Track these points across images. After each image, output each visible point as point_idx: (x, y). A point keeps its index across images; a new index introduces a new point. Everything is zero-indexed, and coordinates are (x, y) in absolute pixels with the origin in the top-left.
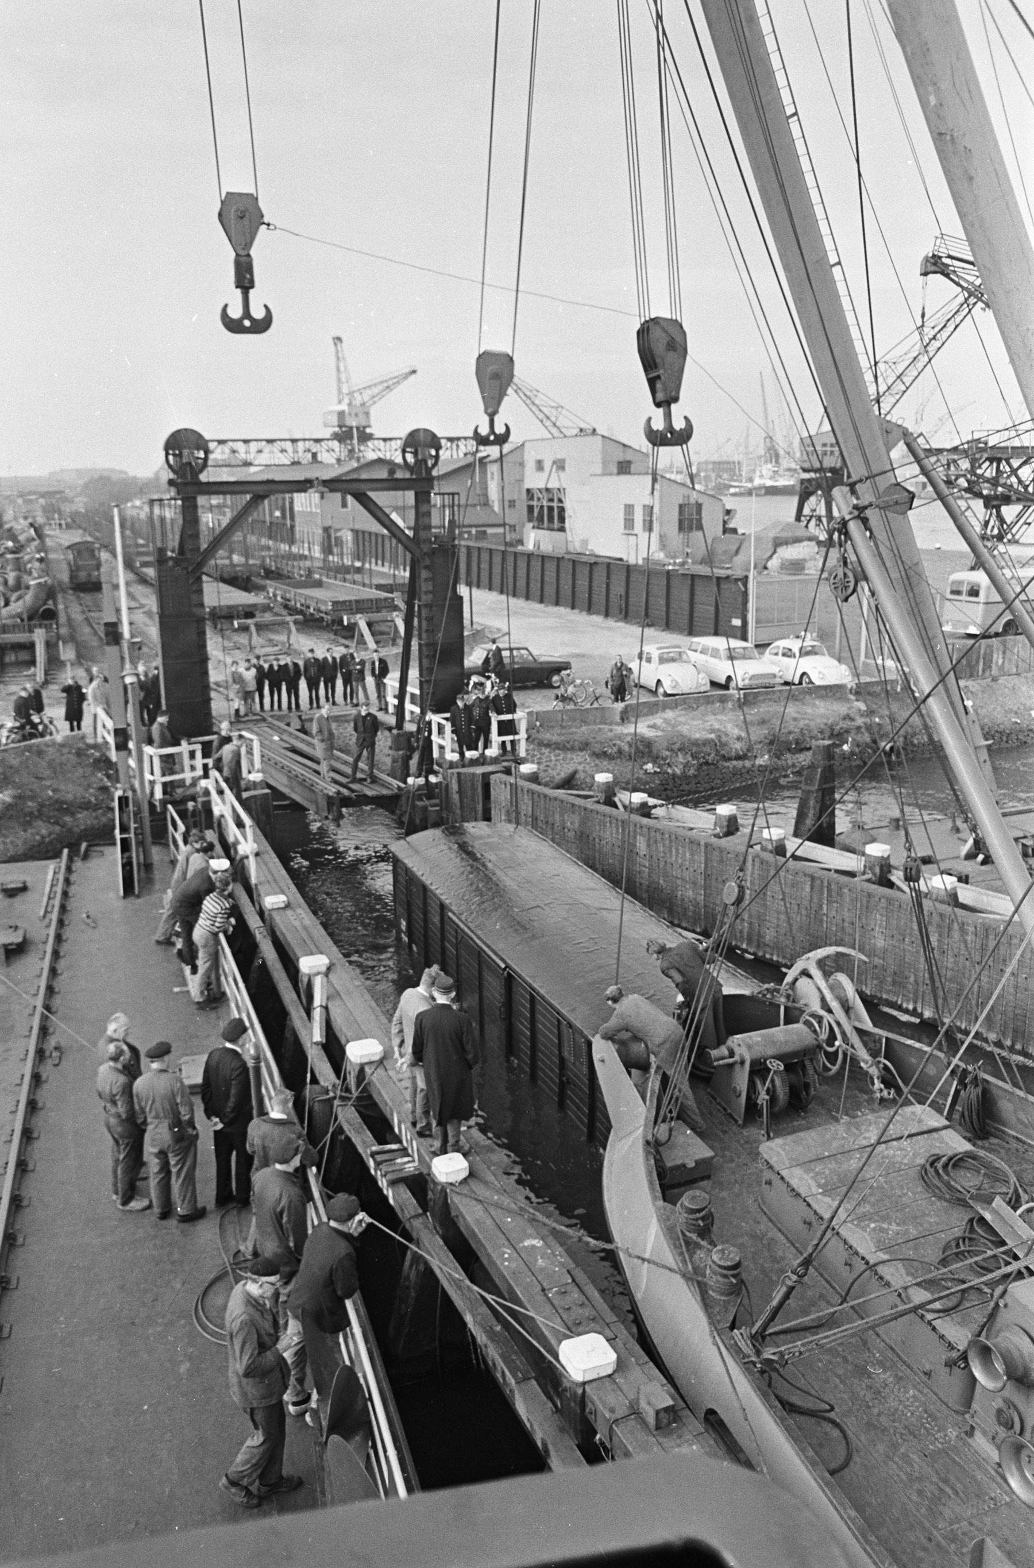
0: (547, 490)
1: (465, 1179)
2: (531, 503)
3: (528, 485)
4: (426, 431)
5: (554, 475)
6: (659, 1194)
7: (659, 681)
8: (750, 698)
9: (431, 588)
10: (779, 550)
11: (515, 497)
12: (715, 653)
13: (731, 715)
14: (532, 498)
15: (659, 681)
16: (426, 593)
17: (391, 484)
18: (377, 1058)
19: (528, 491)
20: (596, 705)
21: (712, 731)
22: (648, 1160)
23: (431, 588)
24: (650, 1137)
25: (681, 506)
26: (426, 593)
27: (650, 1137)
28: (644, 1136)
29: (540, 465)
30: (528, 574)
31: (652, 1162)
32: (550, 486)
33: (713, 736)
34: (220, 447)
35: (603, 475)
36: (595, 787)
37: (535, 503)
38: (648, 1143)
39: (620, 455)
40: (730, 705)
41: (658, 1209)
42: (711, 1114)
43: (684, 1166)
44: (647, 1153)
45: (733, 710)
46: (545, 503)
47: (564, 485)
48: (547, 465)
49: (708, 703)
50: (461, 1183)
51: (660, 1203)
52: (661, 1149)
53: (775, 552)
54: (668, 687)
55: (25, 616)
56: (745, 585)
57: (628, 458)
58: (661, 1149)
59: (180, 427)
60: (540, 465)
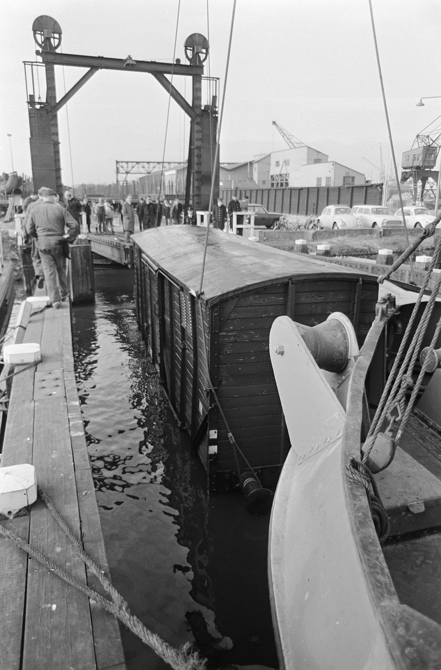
0: (281, 175)
1: (28, 509)
2: (273, 182)
3: (271, 173)
4: (200, 35)
5: (284, 168)
6: (386, 578)
7: (335, 223)
8: (387, 233)
9: (200, 137)
10: (393, 196)
11: (266, 179)
12: (367, 212)
13: (376, 240)
14: (273, 180)
15: (335, 223)
16: (197, 140)
17: (177, 68)
18: (31, 360)
19: (272, 176)
20: (298, 230)
21: (366, 246)
22: (354, 497)
23: (200, 137)
24: (357, 456)
25: (344, 177)
26: (197, 140)
27: (357, 456)
28: (345, 455)
29: (278, 163)
30: (268, 200)
31: (364, 501)
32: (281, 173)
33: (366, 248)
34: (137, 165)
35: (307, 164)
36: (295, 248)
37: (274, 182)
38: (355, 464)
39: (315, 156)
40: (375, 235)
41: (392, 622)
42: (424, 439)
43: (407, 509)
44: (353, 484)
45: (377, 238)
46: (279, 182)
47: (288, 172)
48: (281, 163)
49: (363, 234)
50: (18, 515)
51: (393, 603)
52: (376, 477)
53: (391, 197)
54: (339, 225)
55: (5, 192)
56: (382, 188)
57: (320, 158)
58: (376, 477)
59: (40, 15)
60: (278, 163)
